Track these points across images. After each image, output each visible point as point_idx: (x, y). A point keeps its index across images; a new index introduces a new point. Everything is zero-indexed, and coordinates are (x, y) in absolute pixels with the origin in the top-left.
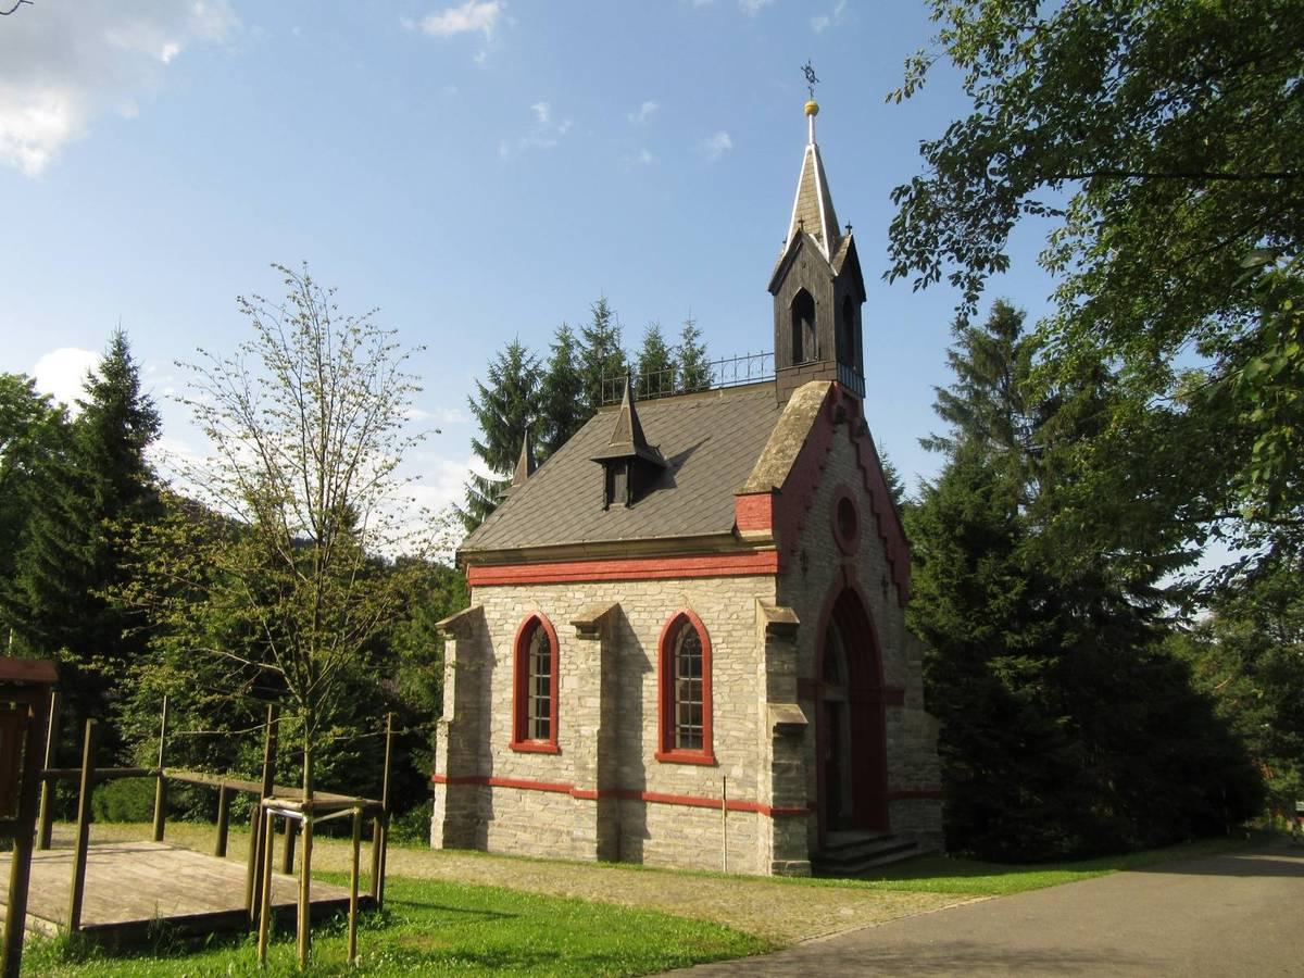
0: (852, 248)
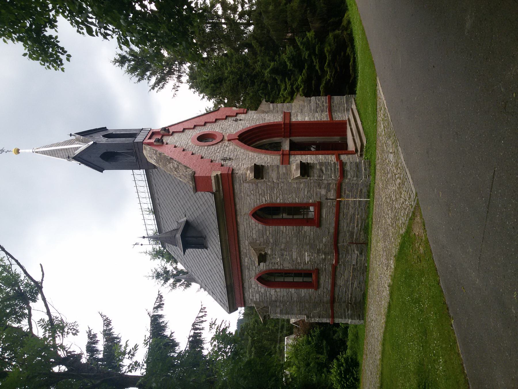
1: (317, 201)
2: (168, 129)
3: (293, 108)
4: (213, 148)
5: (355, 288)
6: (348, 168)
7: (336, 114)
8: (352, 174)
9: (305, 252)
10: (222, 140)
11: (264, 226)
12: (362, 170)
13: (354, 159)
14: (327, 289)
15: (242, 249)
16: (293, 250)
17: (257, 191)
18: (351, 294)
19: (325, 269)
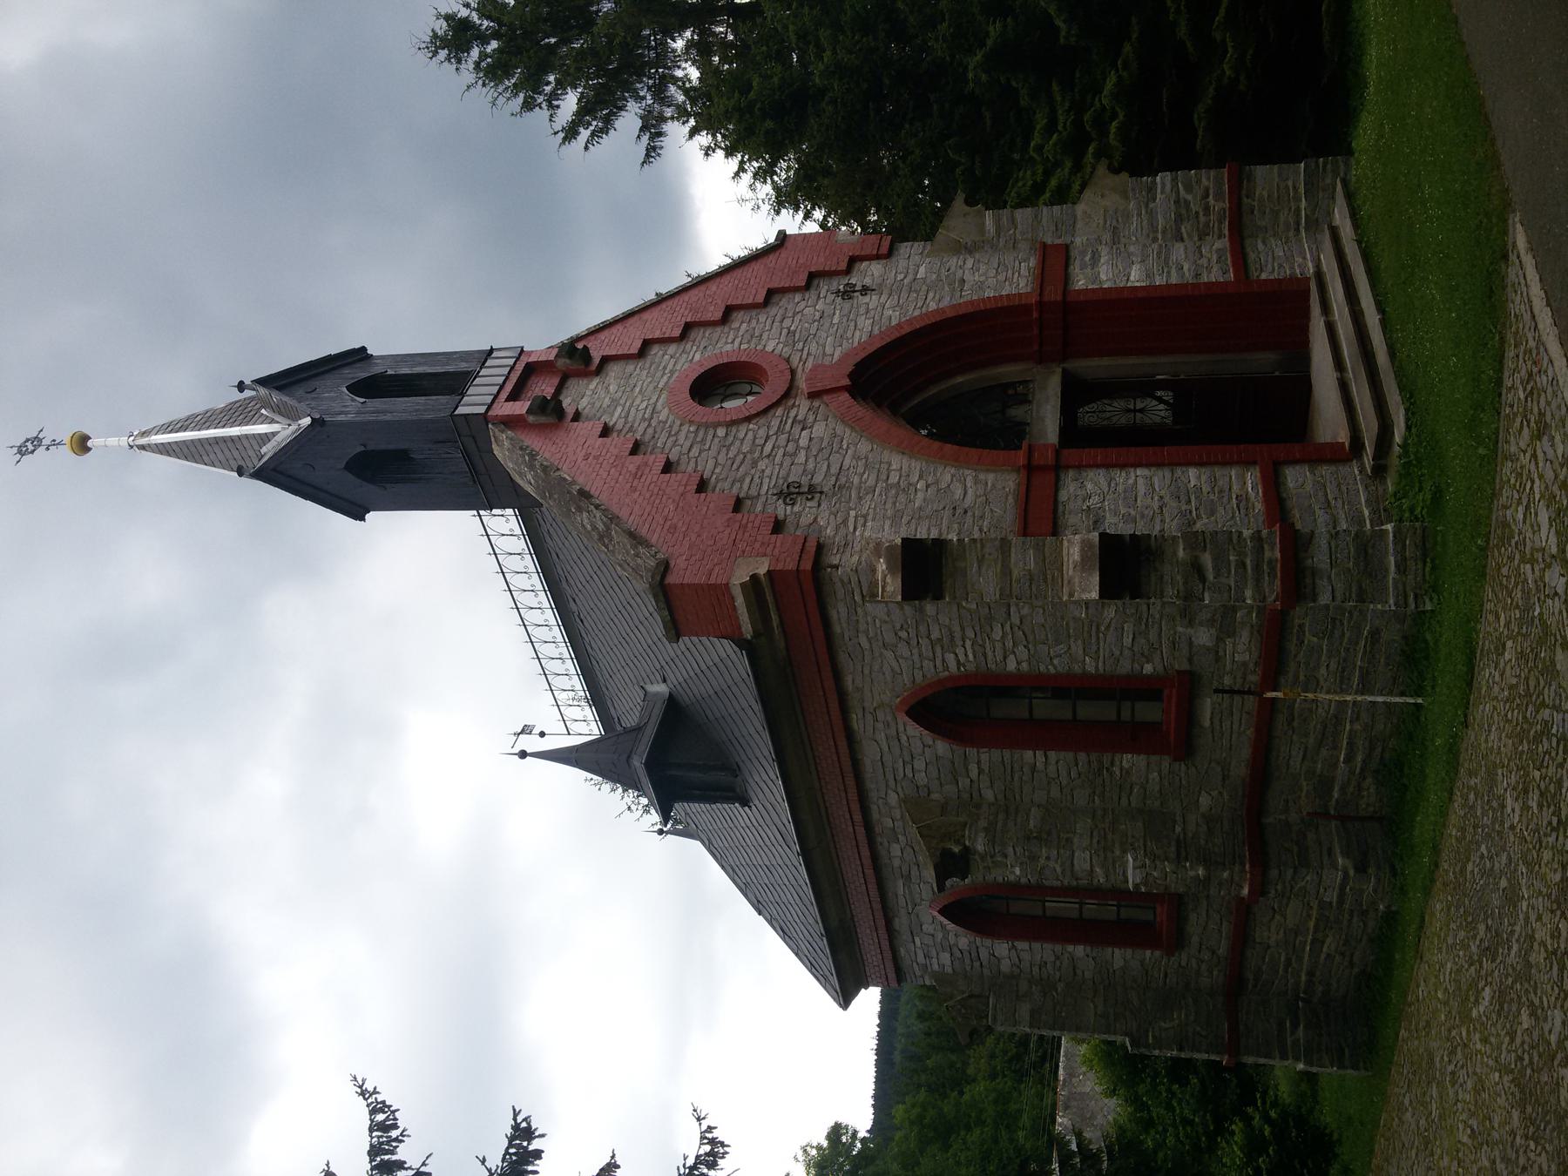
0: (262, 382)
1: (1177, 667)
2: (585, 348)
3: (1079, 225)
4: (750, 434)
5: (1328, 955)
6: (1320, 556)
7: (1264, 242)
8: (1339, 587)
9: (1124, 852)
10: (787, 395)
11: (954, 747)
12: (1387, 571)
13: (1344, 488)
14: (1213, 952)
15: (875, 816)
16: (1075, 840)
17: (922, 629)
18: (1311, 974)
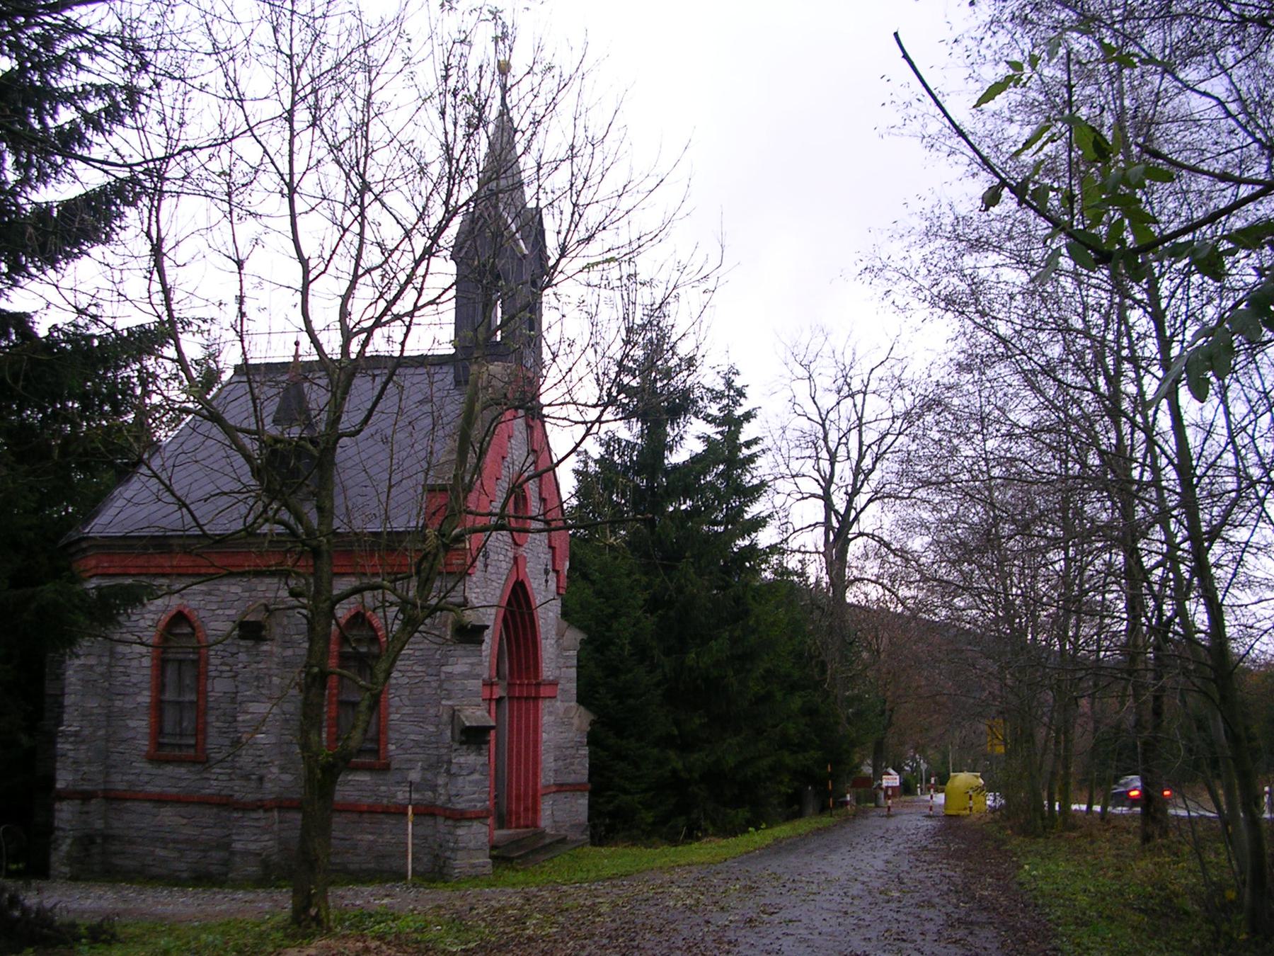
19: (208, 779)
